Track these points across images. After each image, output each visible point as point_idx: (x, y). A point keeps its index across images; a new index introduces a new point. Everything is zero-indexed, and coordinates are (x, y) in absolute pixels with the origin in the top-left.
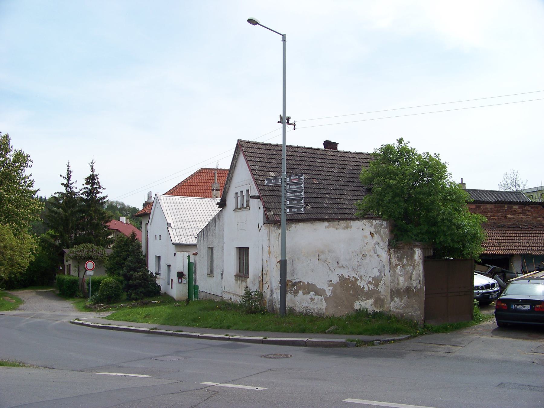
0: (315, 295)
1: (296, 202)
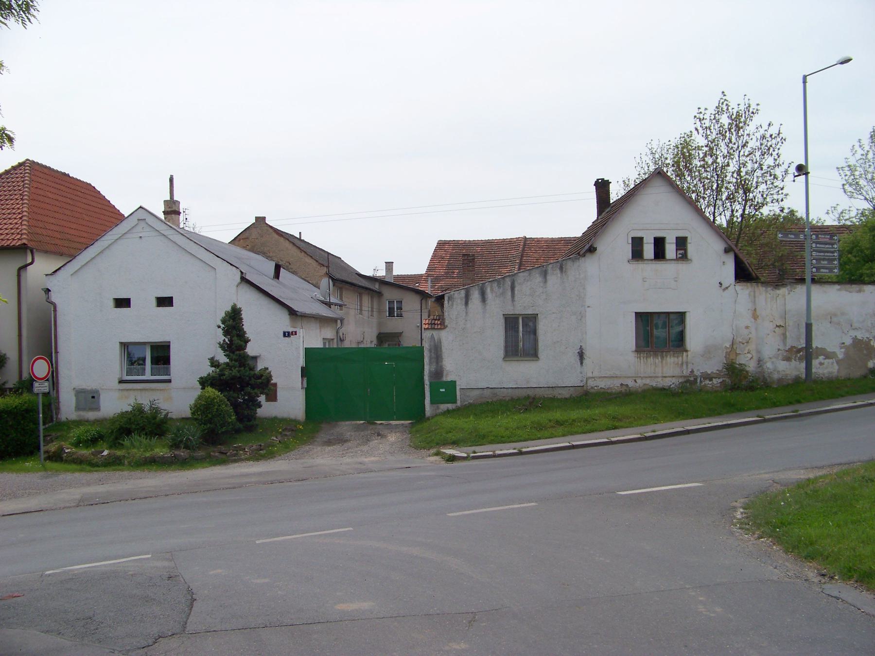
0: (825, 359)
1: (826, 262)
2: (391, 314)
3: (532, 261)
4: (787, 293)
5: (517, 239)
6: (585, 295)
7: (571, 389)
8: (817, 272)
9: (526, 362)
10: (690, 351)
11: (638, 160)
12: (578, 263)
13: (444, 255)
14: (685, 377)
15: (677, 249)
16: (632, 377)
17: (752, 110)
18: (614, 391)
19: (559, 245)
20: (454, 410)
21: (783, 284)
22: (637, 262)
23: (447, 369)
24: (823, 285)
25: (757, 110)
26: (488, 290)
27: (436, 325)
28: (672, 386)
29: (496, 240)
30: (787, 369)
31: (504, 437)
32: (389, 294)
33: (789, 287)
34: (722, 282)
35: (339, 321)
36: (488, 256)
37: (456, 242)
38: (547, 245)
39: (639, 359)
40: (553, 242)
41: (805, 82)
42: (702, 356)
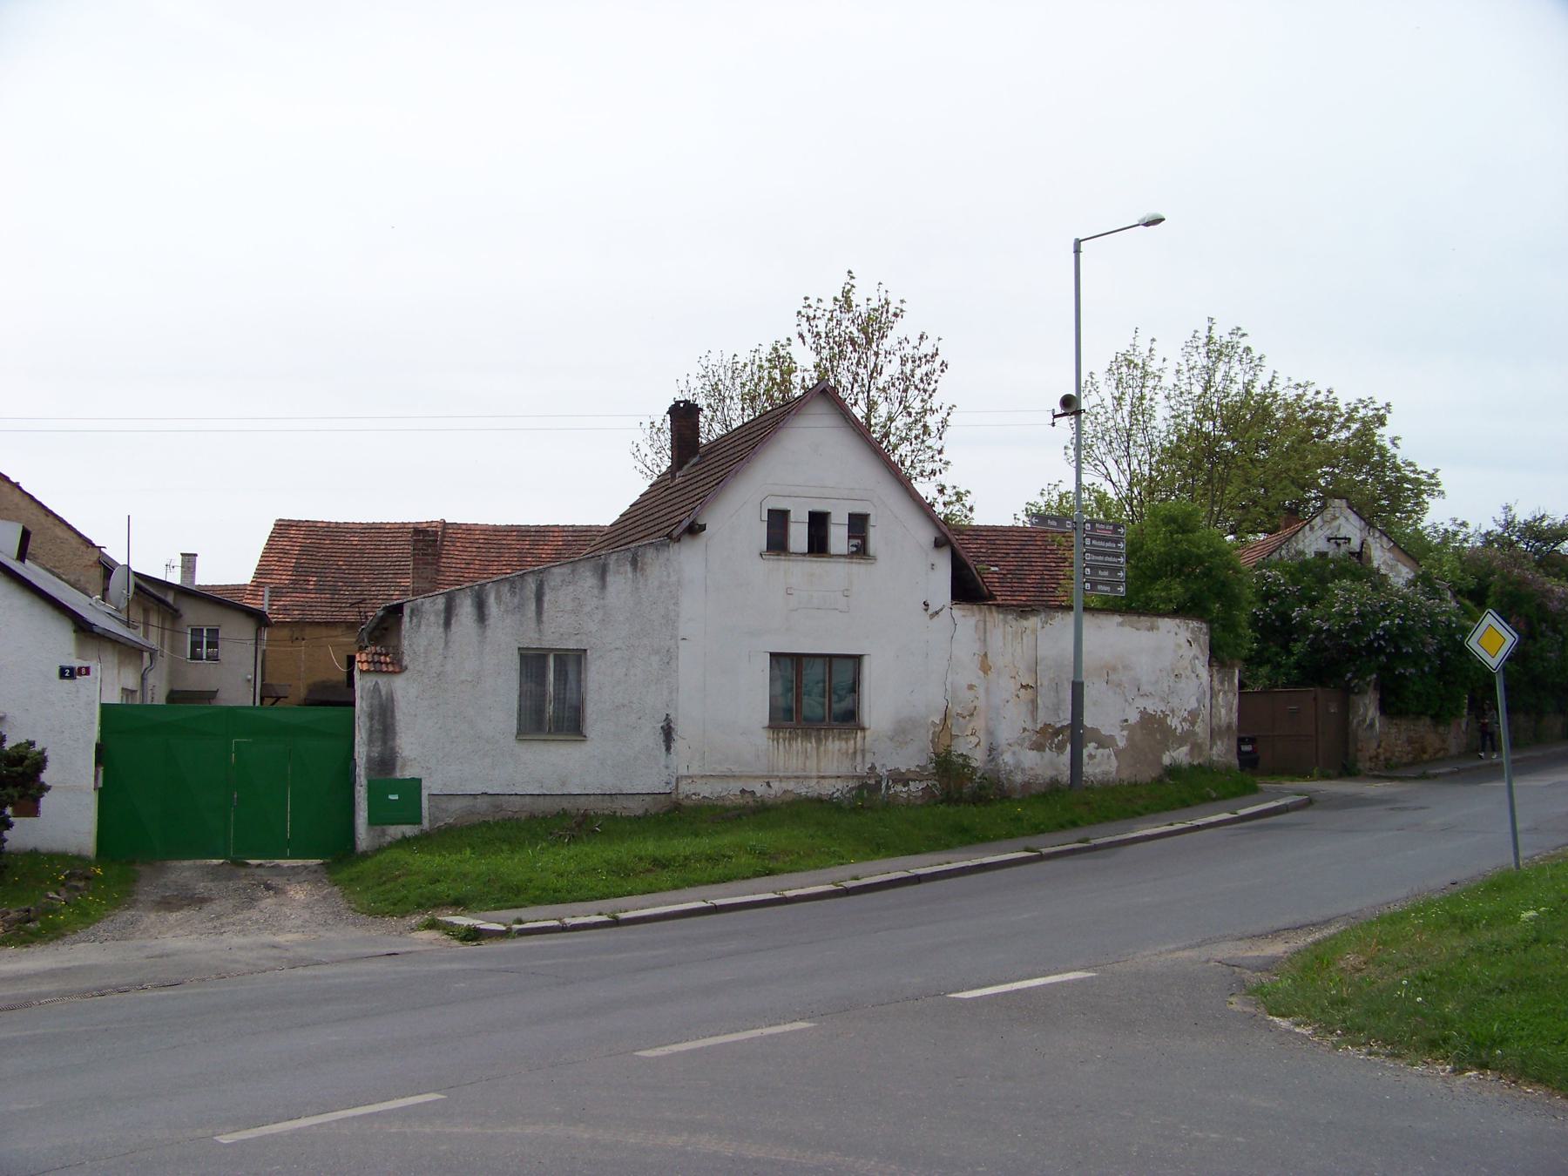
0: (1097, 748)
1: (1106, 573)
2: (195, 656)
3: (458, 566)
4: (1039, 625)
5: (428, 525)
6: (678, 616)
7: (648, 798)
8: (1092, 589)
9: (561, 743)
10: (869, 729)
11: (683, 386)
12: (666, 554)
13: (288, 548)
14: (858, 777)
15: (849, 537)
16: (763, 777)
17: (894, 310)
18: (728, 803)
19: (509, 538)
20: (416, 838)
21: (1034, 610)
22: (776, 557)
23: (403, 755)
24: (1096, 615)
25: (902, 311)
26: (492, 599)
27: (383, 665)
28: (835, 796)
29: (388, 523)
30: (1037, 765)
31: (559, 891)
32: (193, 615)
33: (1043, 615)
34: (929, 602)
35: (146, 655)
36: (374, 553)
37: (311, 524)
38: (486, 537)
39: (775, 742)
40: (497, 533)
41: (1077, 251)
42: (891, 739)
